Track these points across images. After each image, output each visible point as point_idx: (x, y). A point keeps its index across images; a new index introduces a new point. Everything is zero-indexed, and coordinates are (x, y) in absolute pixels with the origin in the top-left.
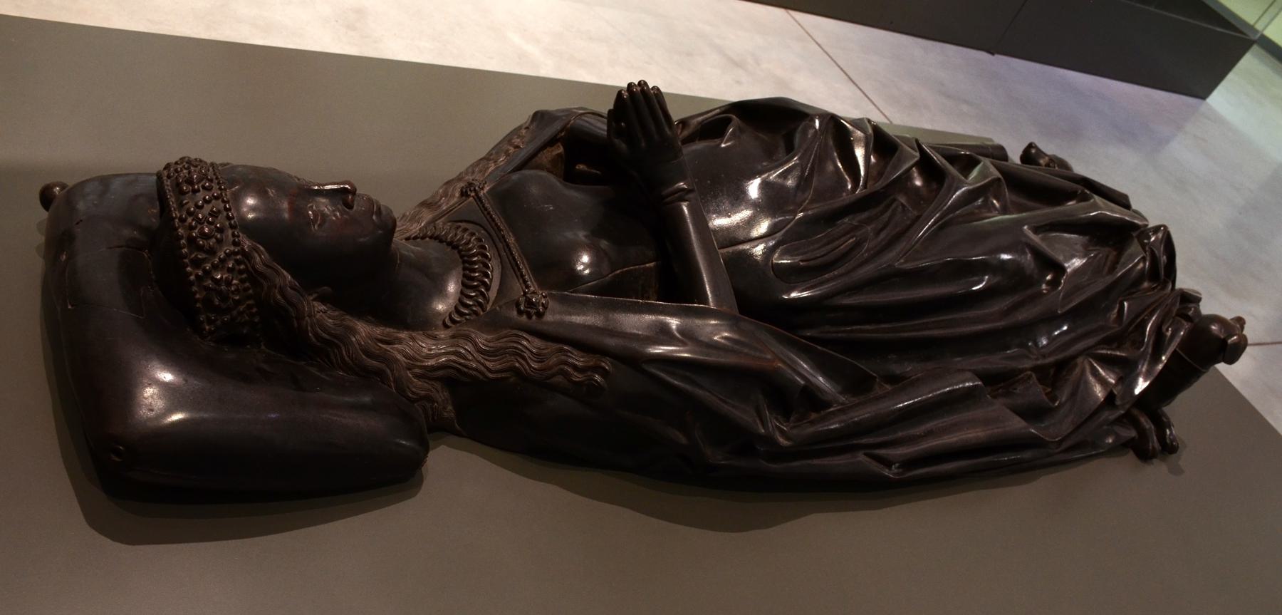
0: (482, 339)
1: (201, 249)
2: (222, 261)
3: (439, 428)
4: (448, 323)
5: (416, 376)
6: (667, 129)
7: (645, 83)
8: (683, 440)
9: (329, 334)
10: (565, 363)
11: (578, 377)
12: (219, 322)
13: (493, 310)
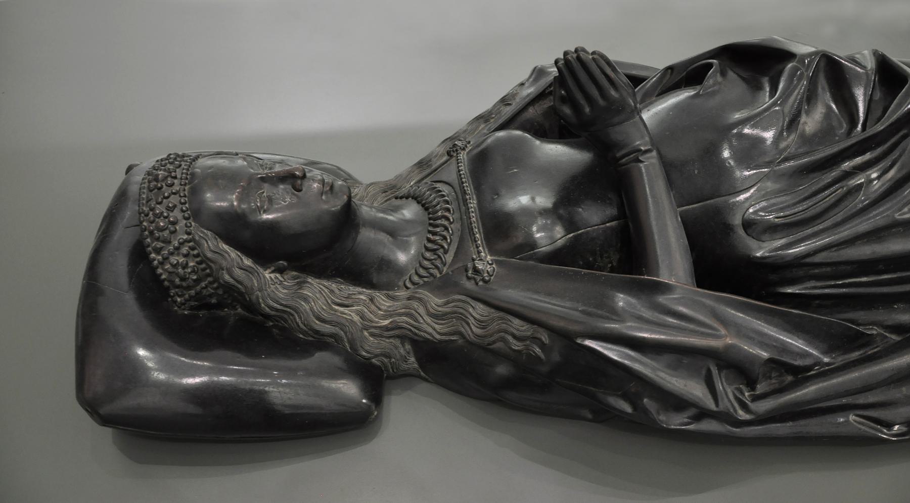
0: (435, 301)
1: (158, 239)
2: (177, 249)
3: (402, 376)
4: (409, 285)
5: (372, 335)
6: (613, 93)
7: (584, 50)
8: (628, 409)
9: (281, 305)
10: (506, 332)
11: (517, 346)
12: (187, 296)
13: (447, 274)
